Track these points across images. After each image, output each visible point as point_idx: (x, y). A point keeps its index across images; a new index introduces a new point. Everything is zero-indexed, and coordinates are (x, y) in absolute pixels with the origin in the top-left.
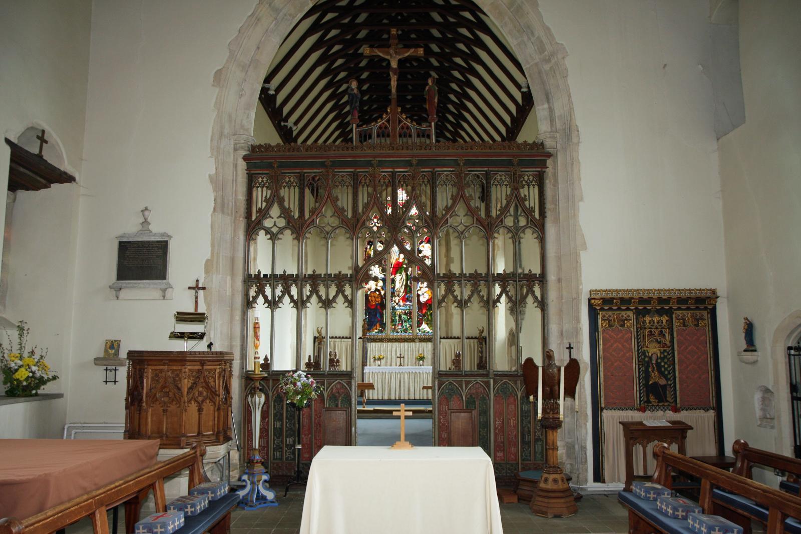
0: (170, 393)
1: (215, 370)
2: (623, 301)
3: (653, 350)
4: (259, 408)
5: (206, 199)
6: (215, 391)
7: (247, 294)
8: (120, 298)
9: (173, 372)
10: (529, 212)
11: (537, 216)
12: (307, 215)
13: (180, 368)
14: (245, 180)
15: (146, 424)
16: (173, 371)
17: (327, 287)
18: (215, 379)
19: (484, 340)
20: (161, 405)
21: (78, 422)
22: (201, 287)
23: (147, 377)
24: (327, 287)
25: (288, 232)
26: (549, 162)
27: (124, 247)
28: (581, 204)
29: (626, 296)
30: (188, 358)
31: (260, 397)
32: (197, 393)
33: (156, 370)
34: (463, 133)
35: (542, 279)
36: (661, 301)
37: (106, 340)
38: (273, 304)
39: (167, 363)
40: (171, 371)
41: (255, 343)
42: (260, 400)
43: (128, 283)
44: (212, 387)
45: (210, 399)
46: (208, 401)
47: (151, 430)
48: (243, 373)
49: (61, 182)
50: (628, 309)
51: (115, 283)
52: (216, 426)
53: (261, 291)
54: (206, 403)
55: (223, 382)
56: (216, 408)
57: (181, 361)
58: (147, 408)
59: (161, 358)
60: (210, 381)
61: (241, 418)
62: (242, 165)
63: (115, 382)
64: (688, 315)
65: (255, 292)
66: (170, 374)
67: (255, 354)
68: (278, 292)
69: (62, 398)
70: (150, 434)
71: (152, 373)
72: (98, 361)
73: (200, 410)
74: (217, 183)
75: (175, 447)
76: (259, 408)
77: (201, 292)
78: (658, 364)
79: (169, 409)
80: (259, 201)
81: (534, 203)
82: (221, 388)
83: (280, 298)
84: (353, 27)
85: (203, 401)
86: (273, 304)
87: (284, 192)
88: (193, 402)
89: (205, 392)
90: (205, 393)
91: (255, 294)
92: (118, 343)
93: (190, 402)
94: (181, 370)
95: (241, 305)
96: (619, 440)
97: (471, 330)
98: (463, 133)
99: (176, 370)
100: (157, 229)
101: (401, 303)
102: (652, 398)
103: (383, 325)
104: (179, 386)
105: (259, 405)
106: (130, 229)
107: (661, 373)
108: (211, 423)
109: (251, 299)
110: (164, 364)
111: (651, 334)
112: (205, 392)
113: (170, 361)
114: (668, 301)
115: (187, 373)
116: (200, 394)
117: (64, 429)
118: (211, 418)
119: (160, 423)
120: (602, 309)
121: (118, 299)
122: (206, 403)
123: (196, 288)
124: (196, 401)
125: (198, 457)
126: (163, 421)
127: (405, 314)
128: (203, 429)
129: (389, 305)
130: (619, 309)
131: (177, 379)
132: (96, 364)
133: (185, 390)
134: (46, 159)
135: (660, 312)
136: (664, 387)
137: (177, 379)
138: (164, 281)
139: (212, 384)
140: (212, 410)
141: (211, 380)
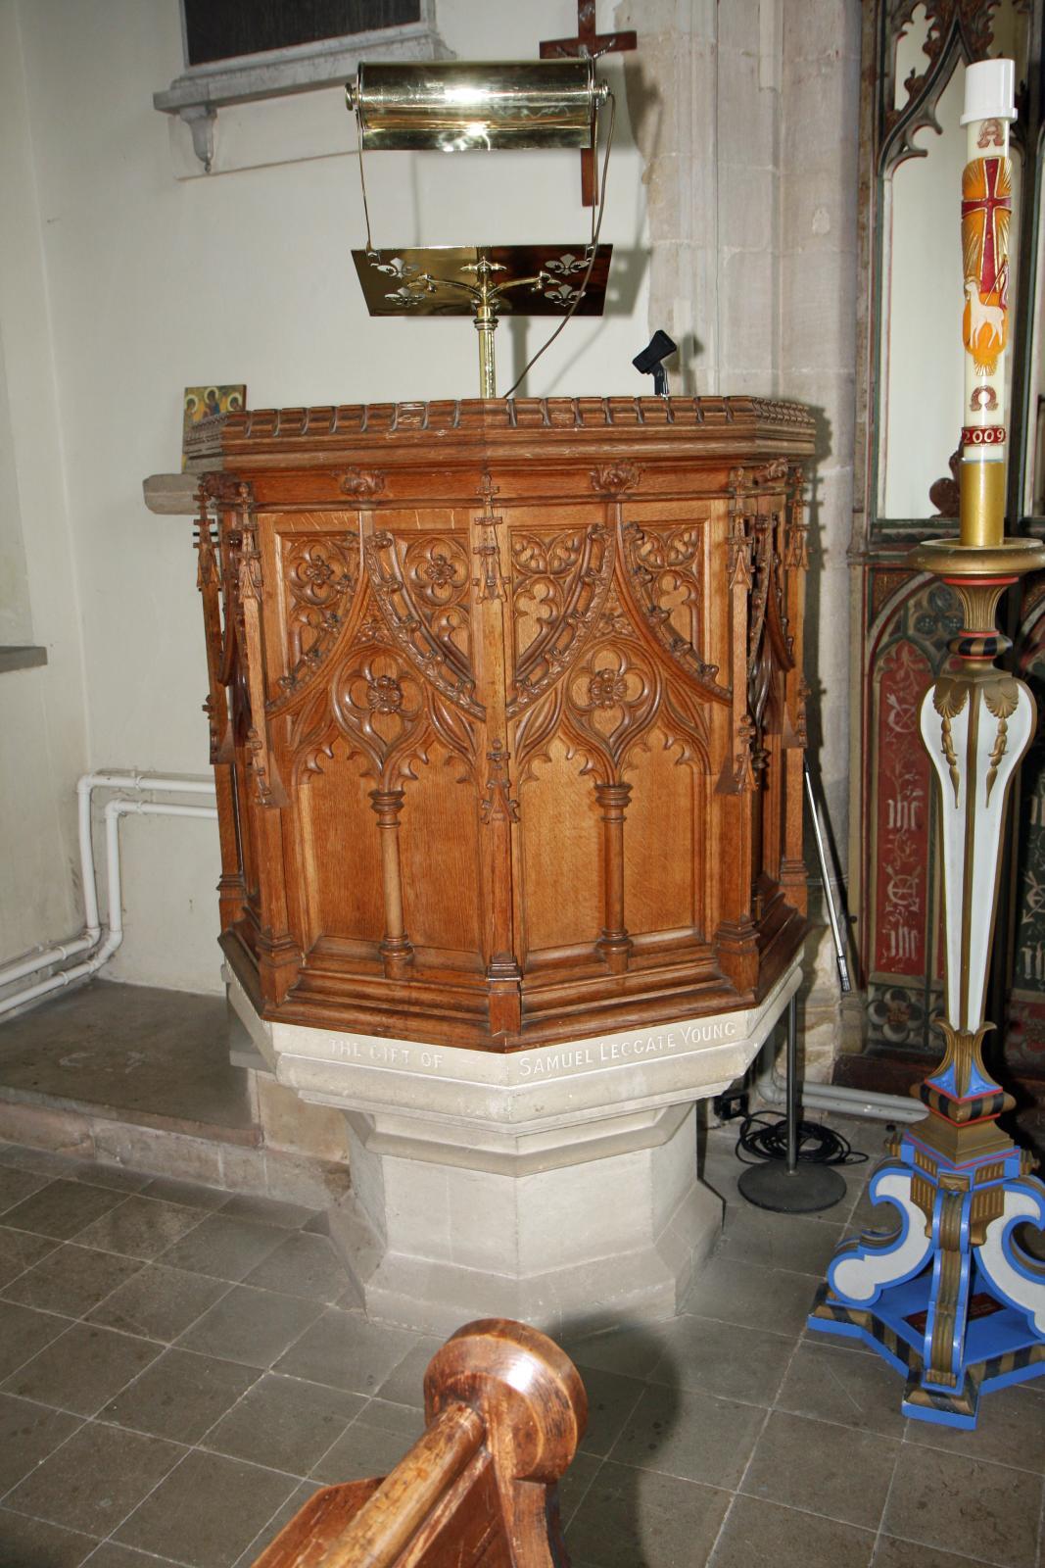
0: (409, 689)
1: (697, 524)
4: (992, 779)
6: (703, 667)
7: (875, 72)
8: (217, 163)
9: (413, 556)
13: (452, 519)
14: (686, 1388)
15: (290, 878)
16: (419, 540)
18: (697, 585)
20: (362, 762)
21: (127, 766)
22: (609, 37)
23: (259, 584)
30: (490, 453)
31: (1004, 709)
32: (582, 683)
33: (313, 538)
37: (188, 391)
39: (370, 492)
40: (403, 546)
41: (976, 325)
42: (1003, 730)
43: (242, 69)
44: (678, 640)
45: (673, 725)
46: (656, 737)
47: (322, 911)
48: (854, 533)
51: (182, 79)
52: (712, 888)
54: (647, 748)
55: (751, 606)
56: (713, 779)
57: (458, 467)
58: (287, 781)
59: (322, 457)
60: (664, 603)
61: (849, 769)
65: (926, 49)
66: (395, 558)
67: (975, 403)
69: (43, 667)
70: (316, 932)
71: (293, 559)
73: (610, 794)
75: (460, 1030)
76: (992, 779)
79: (412, 787)
82: (740, 647)
85: (625, 738)
88: (557, 748)
89: (632, 680)
90: (635, 687)
91: (922, 64)
92: (235, 400)
93: (535, 745)
94: (459, 535)
95: (845, 140)
96: (554, 501)
99: (430, 538)
104: (461, 641)
105: (996, 763)
108: (680, 872)
109: (901, 99)
110: (352, 499)
112: (632, 680)
113: (391, 471)
115: (505, 556)
116: (604, 687)
117: (76, 794)
118: (684, 841)
119: (365, 869)
121: (207, 169)
122: (647, 748)
124: (584, 740)
125: (506, 1489)
126: (382, 865)
128: (633, 911)
131: (443, 594)
132: (156, 508)
133: (493, 671)
137: (443, 594)
138: (409, 29)
139: (681, 622)
140: (683, 788)
141: (672, 597)
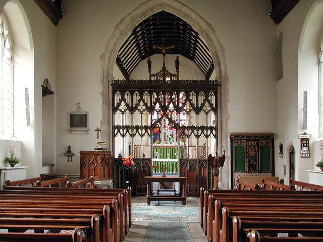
2: (242, 136)
3: (252, 153)
5: (100, 101)
7: (113, 132)
10: (211, 105)
11: (214, 106)
12: (134, 106)
17: (142, 130)
19: (205, 147)
24: (142, 130)
25: (127, 111)
26: (219, 88)
27: (72, 116)
28: (229, 103)
29: (243, 135)
34: (198, 45)
35: (216, 129)
36: (255, 137)
38: (123, 136)
49: (50, 94)
50: (243, 139)
53: (119, 131)
62: (111, 88)
63: (68, 161)
64: (264, 141)
68: (125, 132)
72: (65, 154)
74: (103, 94)
77: (99, 132)
78: (253, 158)
80: (116, 101)
81: (214, 102)
83: (126, 134)
84: (150, 30)
86: (123, 136)
87: (126, 97)
97: (201, 144)
98: (198, 45)
100: (83, 110)
101: (169, 131)
102: (251, 168)
103: (160, 140)
106: (73, 109)
107: (254, 160)
111: (251, 148)
114: (257, 137)
120: (235, 139)
123: (98, 130)
127: (171, 135)
129: (163, 131)
130: (240, 139)
134: (101, 117)
135: (254, 141)
136: (255, 165)
